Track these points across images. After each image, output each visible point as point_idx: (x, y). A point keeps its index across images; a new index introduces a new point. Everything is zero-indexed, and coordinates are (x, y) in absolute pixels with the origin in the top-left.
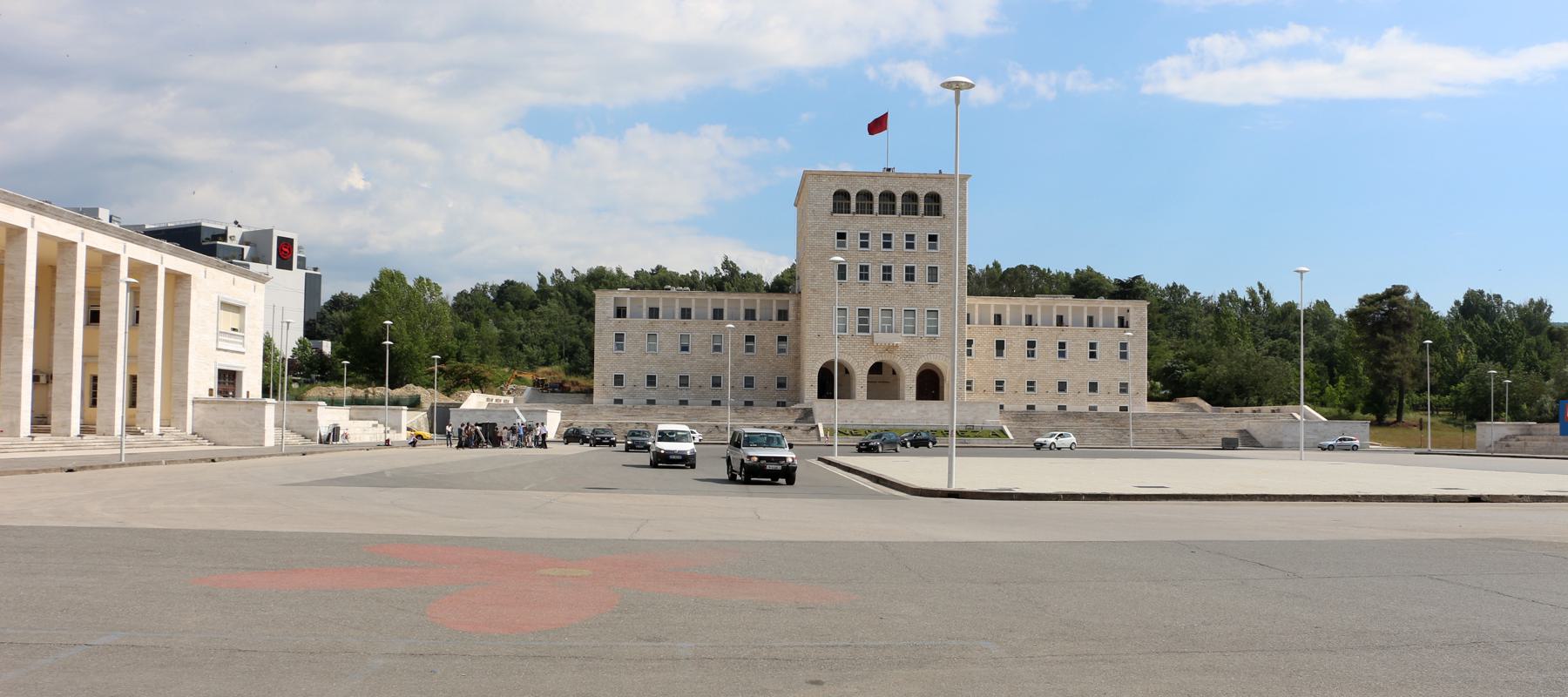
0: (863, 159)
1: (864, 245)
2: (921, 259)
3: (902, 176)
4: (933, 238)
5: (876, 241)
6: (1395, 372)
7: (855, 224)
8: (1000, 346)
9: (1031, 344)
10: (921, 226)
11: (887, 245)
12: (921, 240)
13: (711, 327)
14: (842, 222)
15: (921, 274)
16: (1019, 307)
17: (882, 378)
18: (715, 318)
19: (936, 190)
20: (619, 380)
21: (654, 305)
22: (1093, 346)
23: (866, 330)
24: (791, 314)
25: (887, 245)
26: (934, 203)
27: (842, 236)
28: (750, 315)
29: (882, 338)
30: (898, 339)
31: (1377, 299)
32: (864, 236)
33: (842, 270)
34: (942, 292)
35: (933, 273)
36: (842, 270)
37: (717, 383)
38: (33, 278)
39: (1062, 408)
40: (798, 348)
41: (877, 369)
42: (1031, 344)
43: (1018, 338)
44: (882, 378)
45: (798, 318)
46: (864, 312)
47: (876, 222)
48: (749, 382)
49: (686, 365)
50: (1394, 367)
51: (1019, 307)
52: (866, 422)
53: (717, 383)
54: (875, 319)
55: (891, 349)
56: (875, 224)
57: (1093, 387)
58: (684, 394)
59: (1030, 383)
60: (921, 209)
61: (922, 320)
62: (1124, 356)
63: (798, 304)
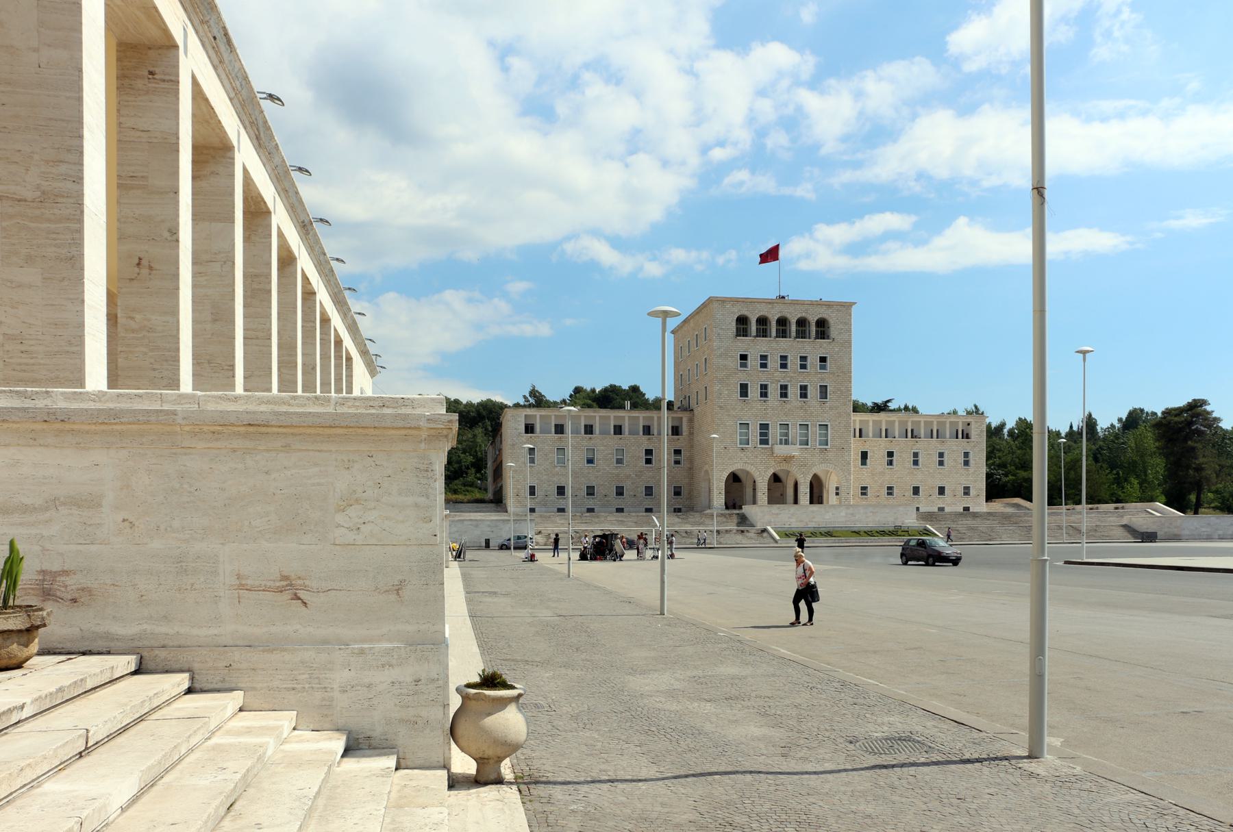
0: (760, 286)
1: (764, 366)
3: (795, 303)
4: (823, 360)
5: (774, 362)
6: (1204, 474)
7: (755, 346)
8: (864, 455)
9: (890, 454)
10: (812, 348)
11: (784, 366)
12: (813, 361)
13: (614, 441)
14: (744, 345)
15: (813, 392)
16: (880, 422)
17: (778, 487)
19: (825, 316)
21: (589, 423)
22: (941, 455)
24: (685, 429)
25: (784, 366)
27: (744, 357)
28: (647, 430)
29: (781, 450)
30: (794, 450)
31: (1179, 411)
32: (764, 357)
33: (744, 390)
34: (831, 408)
35: (824, 391)
36: (744, 390)
37: (561, 491)
40: (691, 460)
41: (776, 478)
42: (890, 454)
43: (878, 450)
44: (778, 487)
45: (691, 434)
46: (764, 427)
47: (774, 345)
48: (591, 491)
49: (592, 476)
50: (1203, 469)
51: (880, 422)
52: (812, 525)
53: (561, 491)
54: (775, 433)
55: (788, 459)
56: (773, 346)
57: (942, 491)
58: (590, 503)
59: (889, 488)
61: (814, 433)
62: (966, 463)
63: (691, 420)
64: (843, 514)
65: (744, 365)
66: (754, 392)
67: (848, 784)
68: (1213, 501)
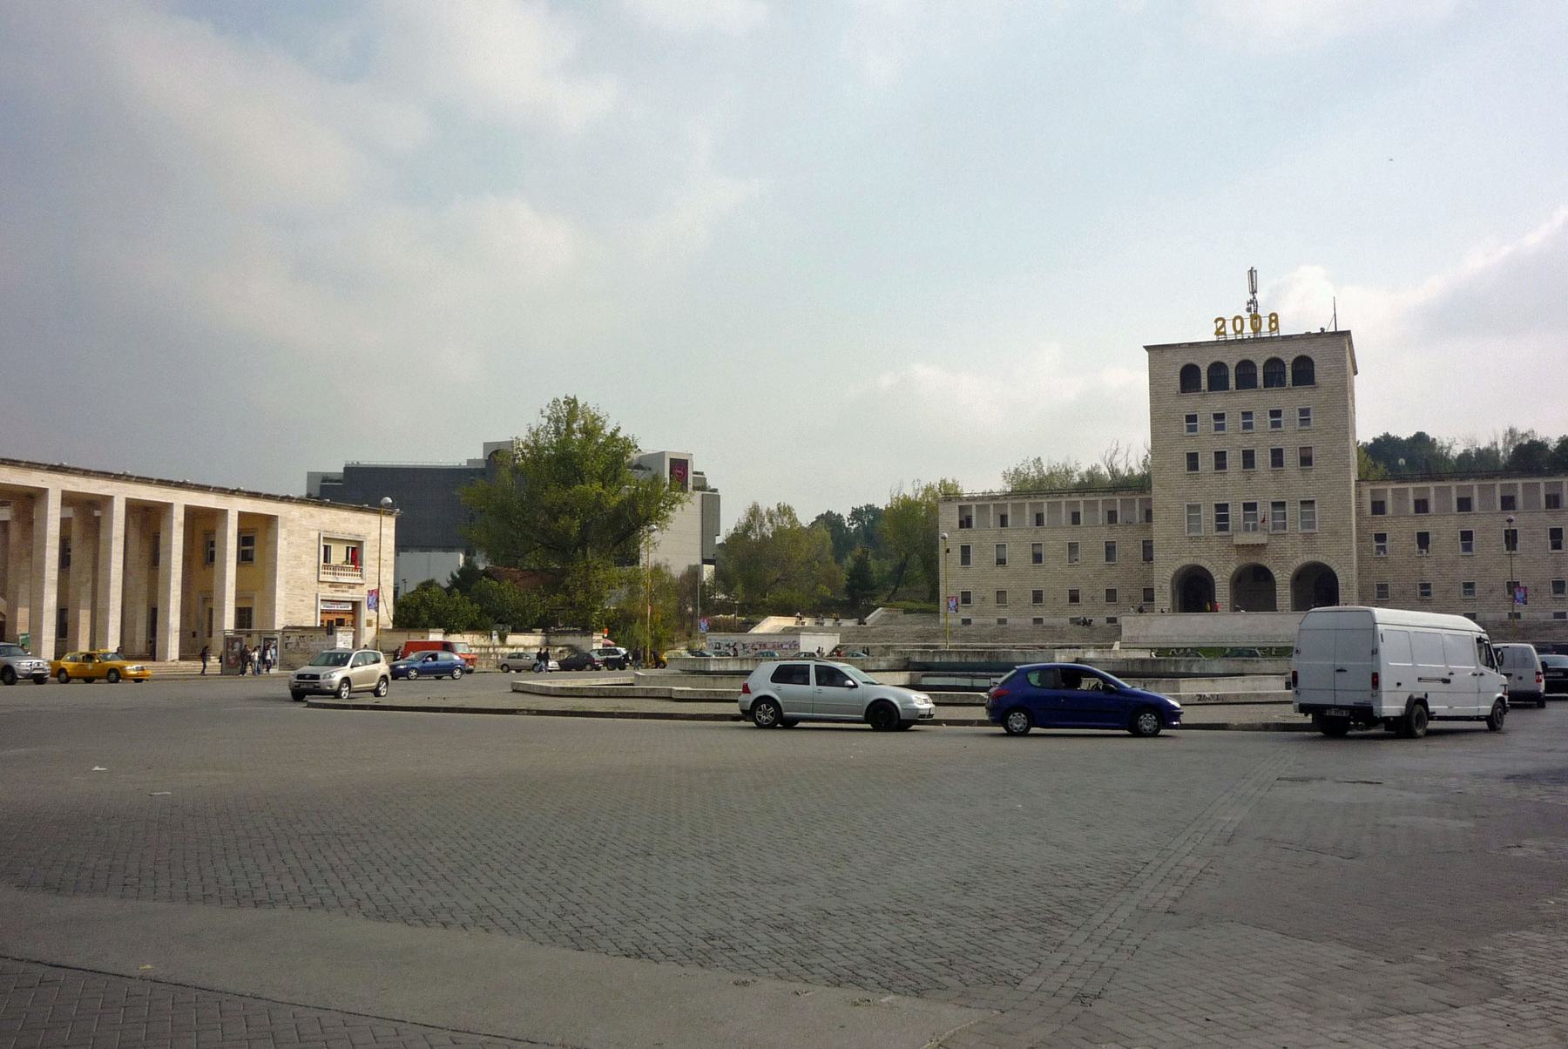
1: (1220, 427)
2: (1290, 440)
7: (1206, 404)
10: (1289, 399)
14: (1191, 403)
15: (1291, 459)
18: (1417, 511)
20: (966, 598)
23: (1225, 528)
26: (1304, 372)
27: (1191, 418)
33: (1193, 460)
36: (1193, 460)
38: (228, 584)
39: (1038, 621)
44: (1254, 588)
46: (1222, 508)
47: (1233, 399)
56: (1232, 402)
60: (1232, 382)
64: (917, 573)
65: (1192, 429)
66: (1206, 463)
67: (375, 595)
68: (392, 506)
